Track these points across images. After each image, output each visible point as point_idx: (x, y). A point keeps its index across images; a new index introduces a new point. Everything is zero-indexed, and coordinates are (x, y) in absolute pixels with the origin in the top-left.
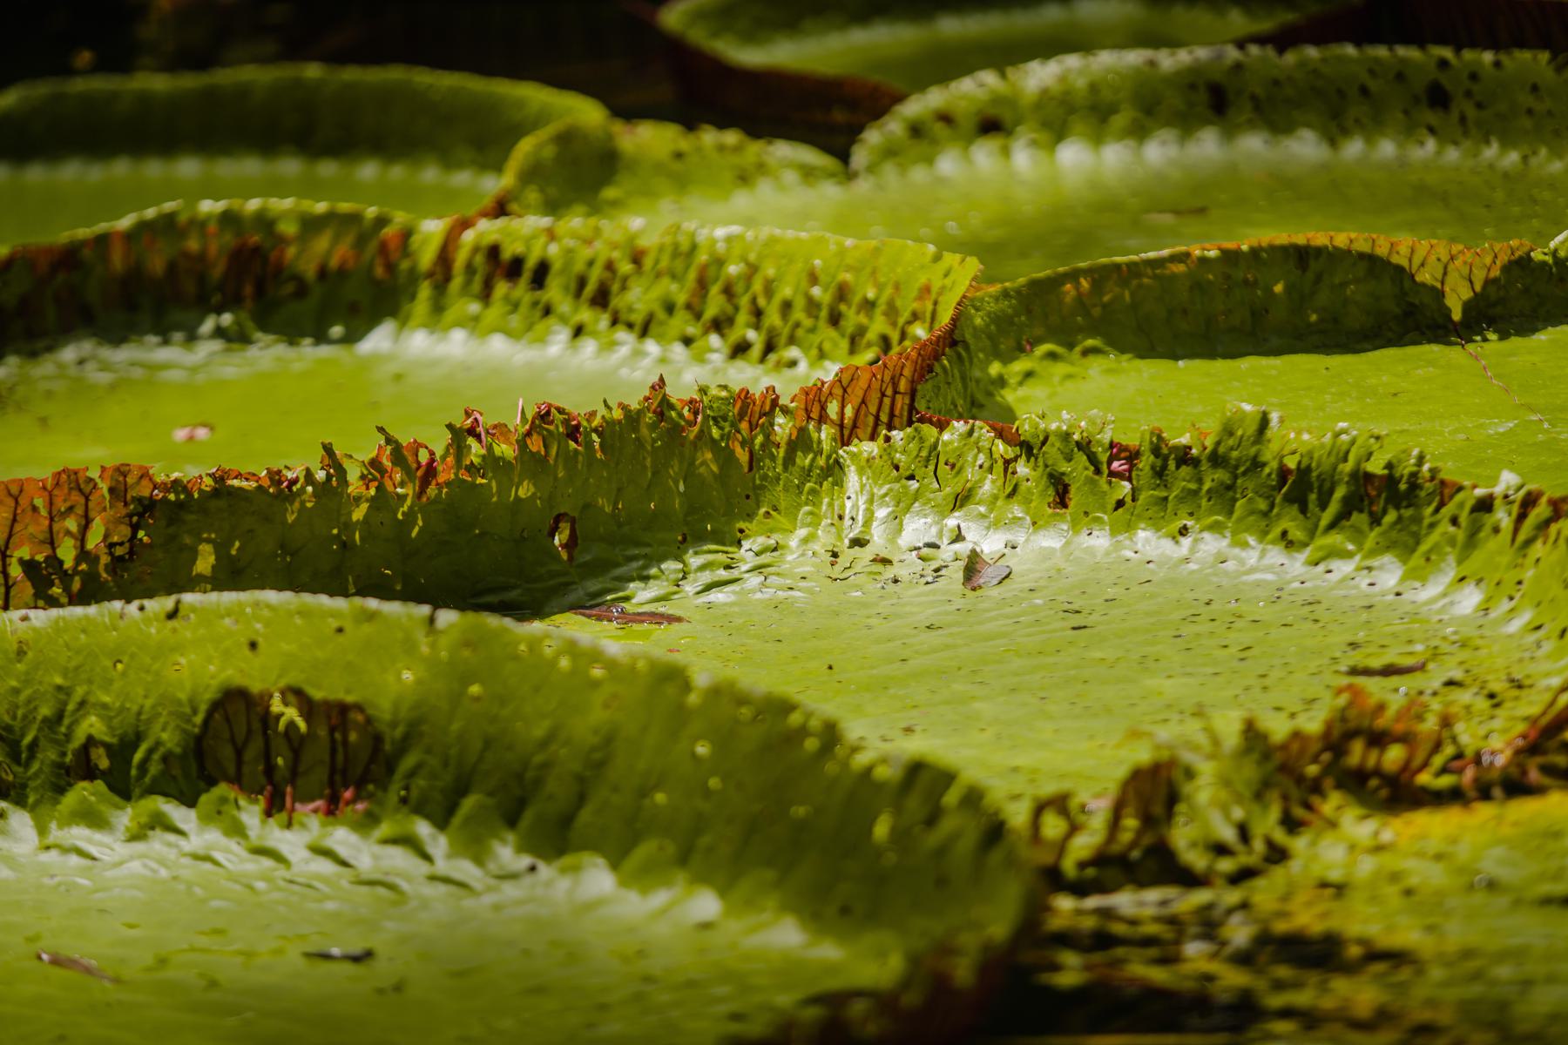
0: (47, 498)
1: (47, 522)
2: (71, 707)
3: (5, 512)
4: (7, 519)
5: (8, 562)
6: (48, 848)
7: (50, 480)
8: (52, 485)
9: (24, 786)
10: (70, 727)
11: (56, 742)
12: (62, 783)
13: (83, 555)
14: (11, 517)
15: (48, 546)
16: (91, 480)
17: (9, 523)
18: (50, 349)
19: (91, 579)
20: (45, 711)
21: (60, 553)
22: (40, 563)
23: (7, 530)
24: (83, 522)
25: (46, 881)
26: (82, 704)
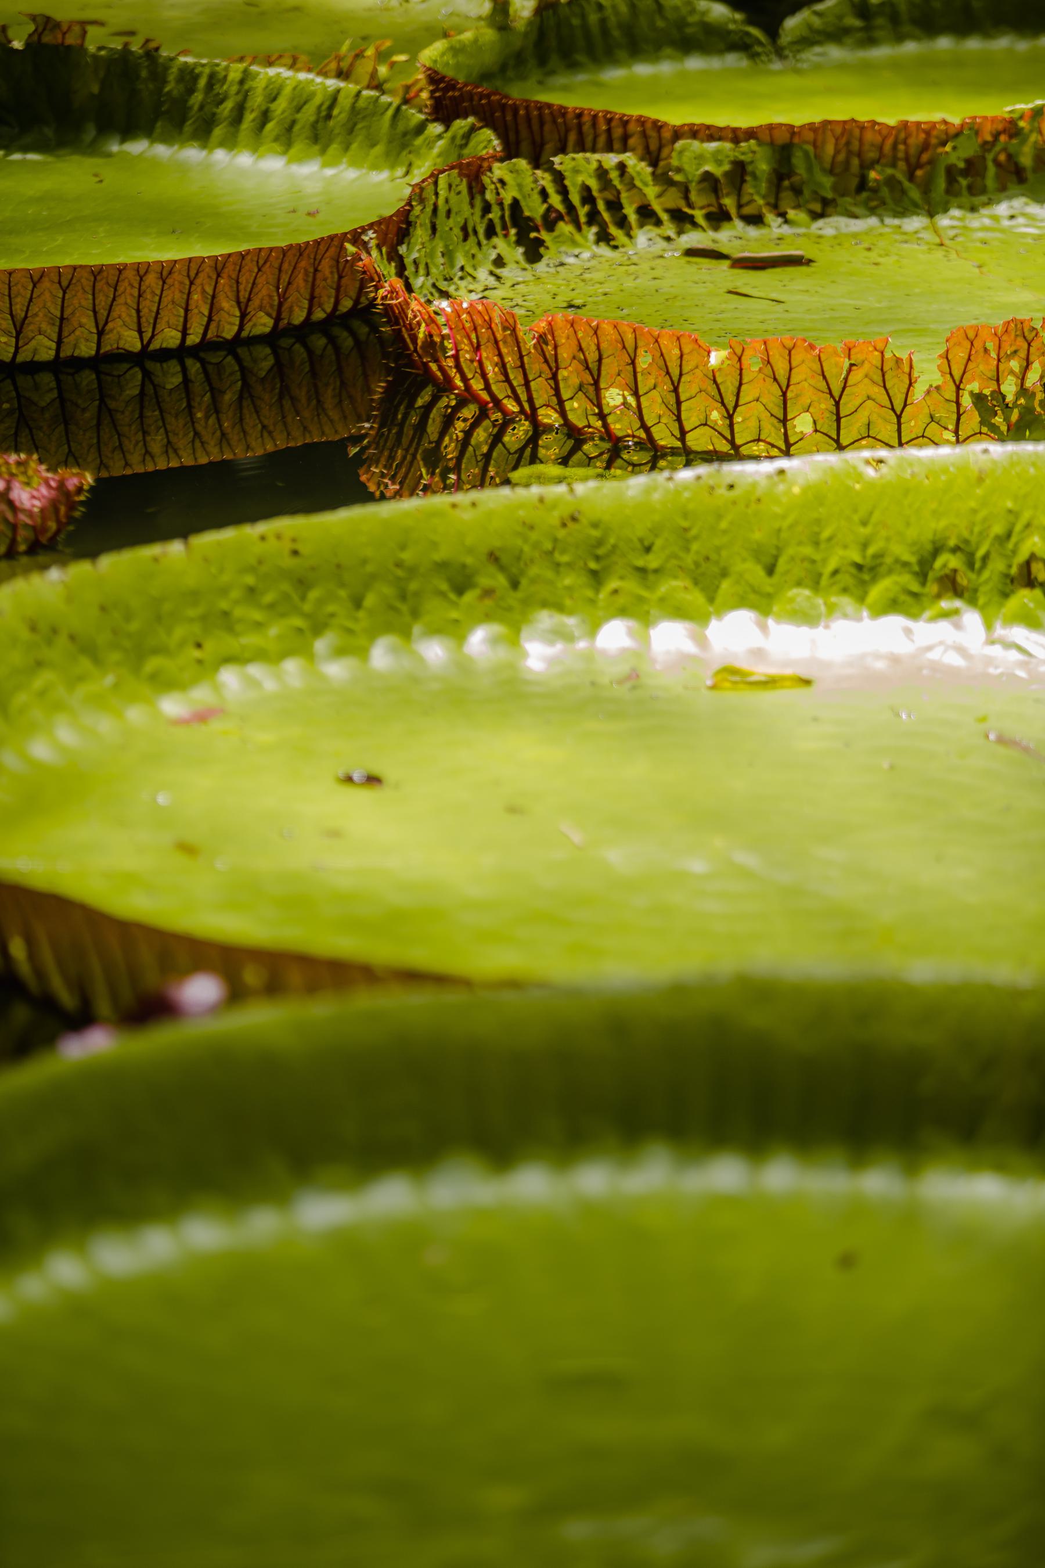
0: (998, 342)
1: (995, 362)
2: (1018, 528)
3: (962, 352)
4: (963, 358)
5: (961, 395)
6: (993, 643)
7: (1001, 327)
8: (1001, 331)
9: (975, 591)
10: (1016, 545)
11: (1006, 556)
12: (1007, 590)
13: (1023, 391)
14: (967, 357)
15: (995, 383)
16: (1034, 329)
17: (965, 361)
18: (989, 203)
19: (1028, 410)
20: (998, 529)
21: (1004, 388)
22: (987, 396)
23: (963, 368)
24: (1025, 364)
25: (991, 670)
26: (1028, 526)
